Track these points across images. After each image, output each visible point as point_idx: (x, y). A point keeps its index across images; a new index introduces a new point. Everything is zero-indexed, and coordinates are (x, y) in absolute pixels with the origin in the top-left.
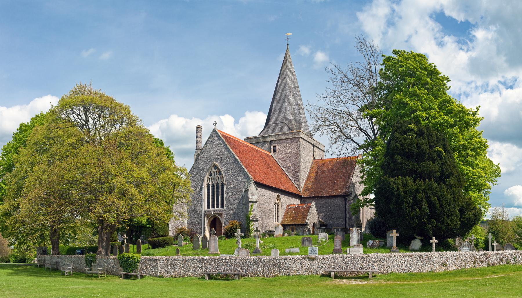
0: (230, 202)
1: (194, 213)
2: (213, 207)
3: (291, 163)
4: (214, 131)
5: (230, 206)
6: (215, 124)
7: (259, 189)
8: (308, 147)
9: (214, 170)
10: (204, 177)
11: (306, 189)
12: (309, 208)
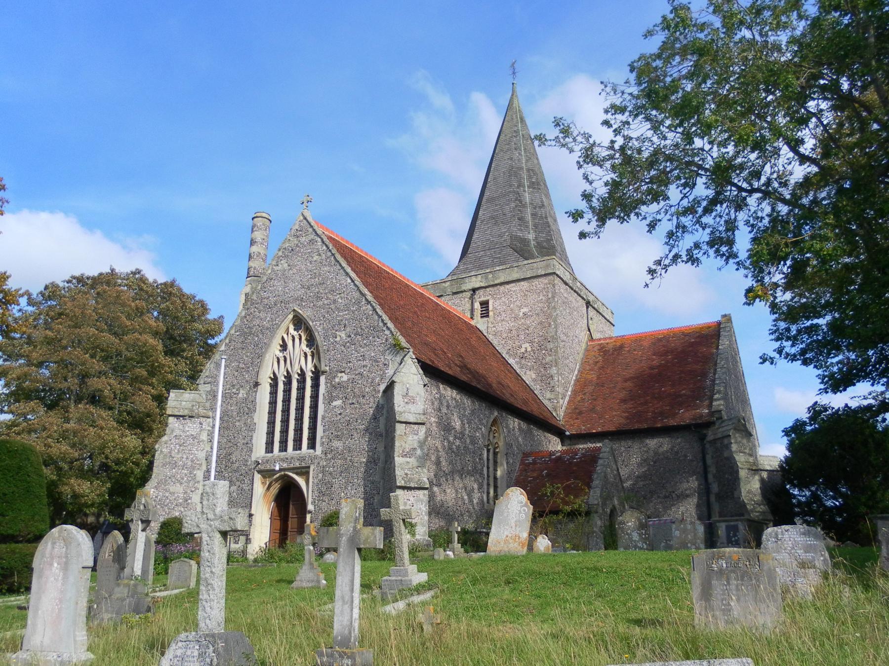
0: (337, 432)
2: (284, 447)
3: (531, 342)
8: (575, 304)
9: (295, 333)
10: (261, 356)
11: (575, 411)
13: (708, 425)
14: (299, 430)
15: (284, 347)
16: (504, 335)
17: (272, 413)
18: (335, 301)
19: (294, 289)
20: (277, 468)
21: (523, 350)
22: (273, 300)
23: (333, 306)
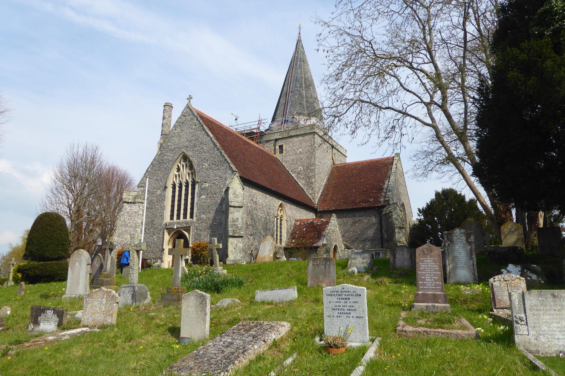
1: (152, 226)
2: (178, 218)
3: (303, 166)
4: (188, 107)
5: (203, 216)
6: (190, 98)
7: (246, 187)
10: (168, 174)
12: (327, 223)
13: (383, 206)
14: (186, 209)
15: (179, 170)
16: (290, 162)
17: (173, 201)
18: (203, 148)
19: (184, 141)
20: (175, 227)
21: (299, 170)
22: (173, 147)
23: (202, 151)
